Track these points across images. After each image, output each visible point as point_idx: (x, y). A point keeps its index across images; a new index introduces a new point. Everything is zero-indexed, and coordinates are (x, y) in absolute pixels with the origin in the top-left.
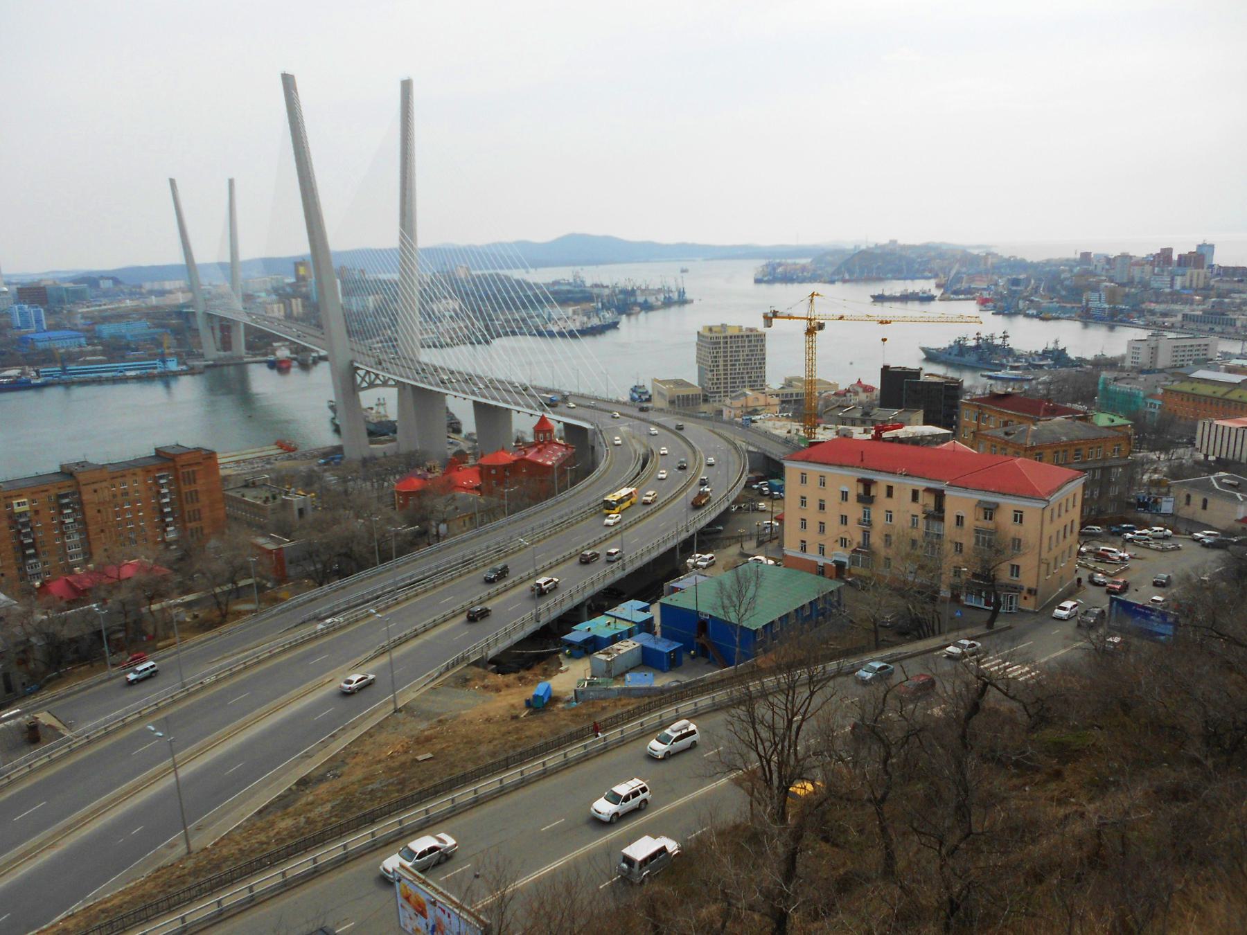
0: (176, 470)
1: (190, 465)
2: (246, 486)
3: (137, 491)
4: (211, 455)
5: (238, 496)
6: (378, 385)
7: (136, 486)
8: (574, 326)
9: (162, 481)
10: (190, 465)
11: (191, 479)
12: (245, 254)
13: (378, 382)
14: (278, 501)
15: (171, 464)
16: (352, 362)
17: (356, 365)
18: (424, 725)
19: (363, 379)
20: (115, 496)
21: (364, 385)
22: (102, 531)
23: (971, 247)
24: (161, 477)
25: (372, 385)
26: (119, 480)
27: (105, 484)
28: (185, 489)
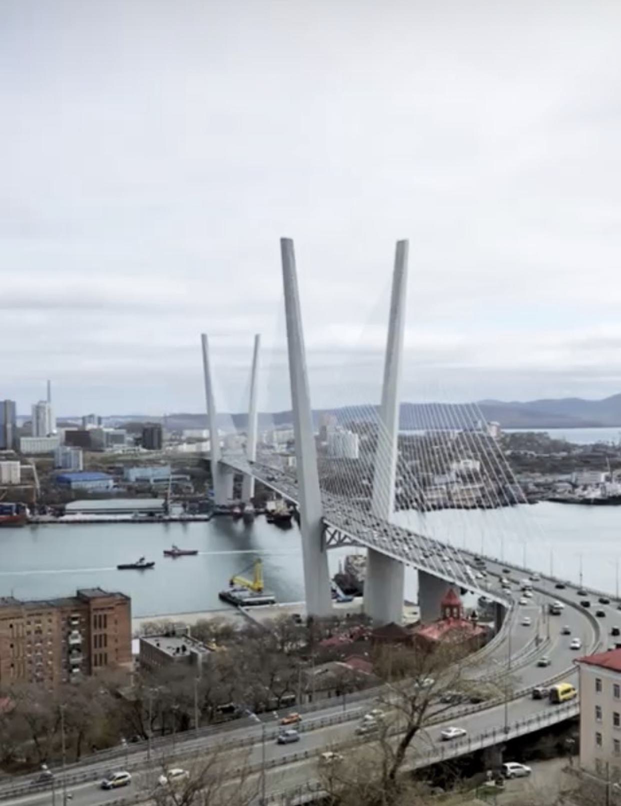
0: (89, 613)
1: (102, 609)
2: (167, 635)
3: (50, 630)
4: (125, 601)
5: (155, 645)
6: (347, 544)
7: (51, 625)
8: (596, 494)
9: (75, 623)
10: (102, 609)
11: (102, 622)
12: (320, 399)
13: (347, 540)
14: (187, 653)
15: (84, 607)
16: (323, 518)
17: (325, 521)
18: (342, 786)
19: (333, 536)
20: (29, 633)
21: (333, 542)
22: (12, 665)
23: (69, 418)
24: (75, 619)
25: (340, 543)
26: (36, 618)
27: (19, 621)
28: (95, 632)
